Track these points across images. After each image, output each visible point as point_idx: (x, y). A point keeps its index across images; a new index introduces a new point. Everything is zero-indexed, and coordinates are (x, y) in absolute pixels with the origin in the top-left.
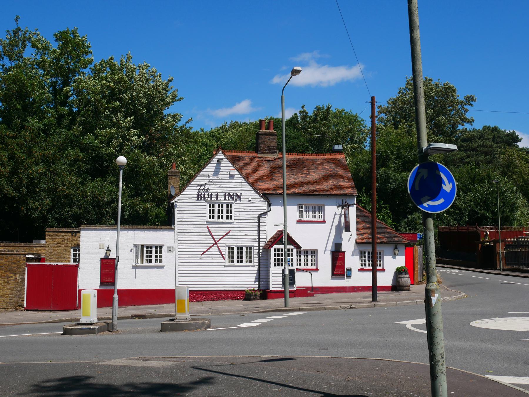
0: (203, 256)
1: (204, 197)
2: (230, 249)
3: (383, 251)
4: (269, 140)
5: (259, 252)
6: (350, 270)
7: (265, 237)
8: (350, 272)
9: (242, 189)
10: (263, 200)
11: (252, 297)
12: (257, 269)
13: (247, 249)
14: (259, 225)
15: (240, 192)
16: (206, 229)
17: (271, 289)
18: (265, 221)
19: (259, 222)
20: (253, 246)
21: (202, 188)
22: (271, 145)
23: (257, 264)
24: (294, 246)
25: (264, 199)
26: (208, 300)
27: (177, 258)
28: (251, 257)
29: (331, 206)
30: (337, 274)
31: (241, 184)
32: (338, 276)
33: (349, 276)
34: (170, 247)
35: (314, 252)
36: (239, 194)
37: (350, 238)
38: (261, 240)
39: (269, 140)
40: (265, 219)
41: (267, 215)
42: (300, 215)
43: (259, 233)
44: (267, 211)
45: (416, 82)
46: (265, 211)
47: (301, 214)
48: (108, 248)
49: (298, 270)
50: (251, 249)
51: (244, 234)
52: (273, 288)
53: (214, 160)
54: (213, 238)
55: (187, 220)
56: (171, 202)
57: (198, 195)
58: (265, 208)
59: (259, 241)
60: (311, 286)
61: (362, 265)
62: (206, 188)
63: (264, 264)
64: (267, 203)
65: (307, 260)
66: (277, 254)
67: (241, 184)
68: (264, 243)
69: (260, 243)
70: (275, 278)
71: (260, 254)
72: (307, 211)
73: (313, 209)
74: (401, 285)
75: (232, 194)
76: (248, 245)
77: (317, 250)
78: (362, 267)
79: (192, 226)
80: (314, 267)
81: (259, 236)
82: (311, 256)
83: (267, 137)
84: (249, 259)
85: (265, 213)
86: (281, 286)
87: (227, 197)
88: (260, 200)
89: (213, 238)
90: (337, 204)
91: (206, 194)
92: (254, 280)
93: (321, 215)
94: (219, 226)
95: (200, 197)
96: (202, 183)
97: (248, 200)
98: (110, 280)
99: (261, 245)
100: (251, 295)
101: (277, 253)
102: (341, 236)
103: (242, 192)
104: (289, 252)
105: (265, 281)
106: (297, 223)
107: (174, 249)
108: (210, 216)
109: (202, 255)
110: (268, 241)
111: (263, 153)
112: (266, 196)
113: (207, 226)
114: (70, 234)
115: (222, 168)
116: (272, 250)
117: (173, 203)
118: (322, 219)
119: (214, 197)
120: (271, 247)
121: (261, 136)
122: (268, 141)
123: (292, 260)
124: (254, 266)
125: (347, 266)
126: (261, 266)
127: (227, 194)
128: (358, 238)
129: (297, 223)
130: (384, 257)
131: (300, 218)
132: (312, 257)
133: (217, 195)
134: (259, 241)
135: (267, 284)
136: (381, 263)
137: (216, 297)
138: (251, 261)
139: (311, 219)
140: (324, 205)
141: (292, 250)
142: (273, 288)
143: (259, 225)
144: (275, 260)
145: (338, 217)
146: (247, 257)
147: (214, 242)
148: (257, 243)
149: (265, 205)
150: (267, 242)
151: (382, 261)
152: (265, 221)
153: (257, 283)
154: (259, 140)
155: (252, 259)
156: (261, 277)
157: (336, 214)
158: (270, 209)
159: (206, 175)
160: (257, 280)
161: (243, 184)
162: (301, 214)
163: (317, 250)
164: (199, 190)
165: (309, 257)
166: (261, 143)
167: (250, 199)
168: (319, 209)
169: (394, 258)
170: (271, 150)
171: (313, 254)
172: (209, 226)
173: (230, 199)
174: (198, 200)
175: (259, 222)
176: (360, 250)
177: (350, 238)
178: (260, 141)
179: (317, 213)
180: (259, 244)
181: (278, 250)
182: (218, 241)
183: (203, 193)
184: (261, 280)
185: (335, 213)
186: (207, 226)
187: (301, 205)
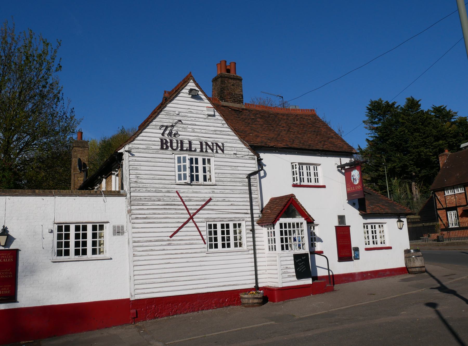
0: (173, 238)
1: (171, 146)
2: (212, 227)
4: (233, 85)
6: (357, 249)
10: (252, 154)
16: (176, 195)
21: (167, 132)
22: (236, 92)
33: (357, 258)
34: (118, 227)
36: (220, 144)
39: (233, 85)
48: (190, 73)
53: (183, 91)
56: (119, 152)
57: (162, 140)
58: (254, 165)
59: (252, 214)
62: (174, 132)
66: (313, 238)
75: (210, 143)
83: (230, 81)
85: (254, 173)
86: (295, 278)
87: (204, 147)
88: (247, 153)
91: (175, 141)
95: (164, 145)
96: (166, 124)
97: (232, 152)
98: (6, 292)
108: (180, 176)
109: (171, 237)
119: (186, 146)
122: (232, 87)
125: (353, 245)
127: (204, 144)
133: (190, 143)
134: (252, 214)
147: (188, 216)
164: (163, 134)
170: (236, 98)
173: (209, 151)
174: (162, 148)
182: (195, 214)
183: (169, 141)
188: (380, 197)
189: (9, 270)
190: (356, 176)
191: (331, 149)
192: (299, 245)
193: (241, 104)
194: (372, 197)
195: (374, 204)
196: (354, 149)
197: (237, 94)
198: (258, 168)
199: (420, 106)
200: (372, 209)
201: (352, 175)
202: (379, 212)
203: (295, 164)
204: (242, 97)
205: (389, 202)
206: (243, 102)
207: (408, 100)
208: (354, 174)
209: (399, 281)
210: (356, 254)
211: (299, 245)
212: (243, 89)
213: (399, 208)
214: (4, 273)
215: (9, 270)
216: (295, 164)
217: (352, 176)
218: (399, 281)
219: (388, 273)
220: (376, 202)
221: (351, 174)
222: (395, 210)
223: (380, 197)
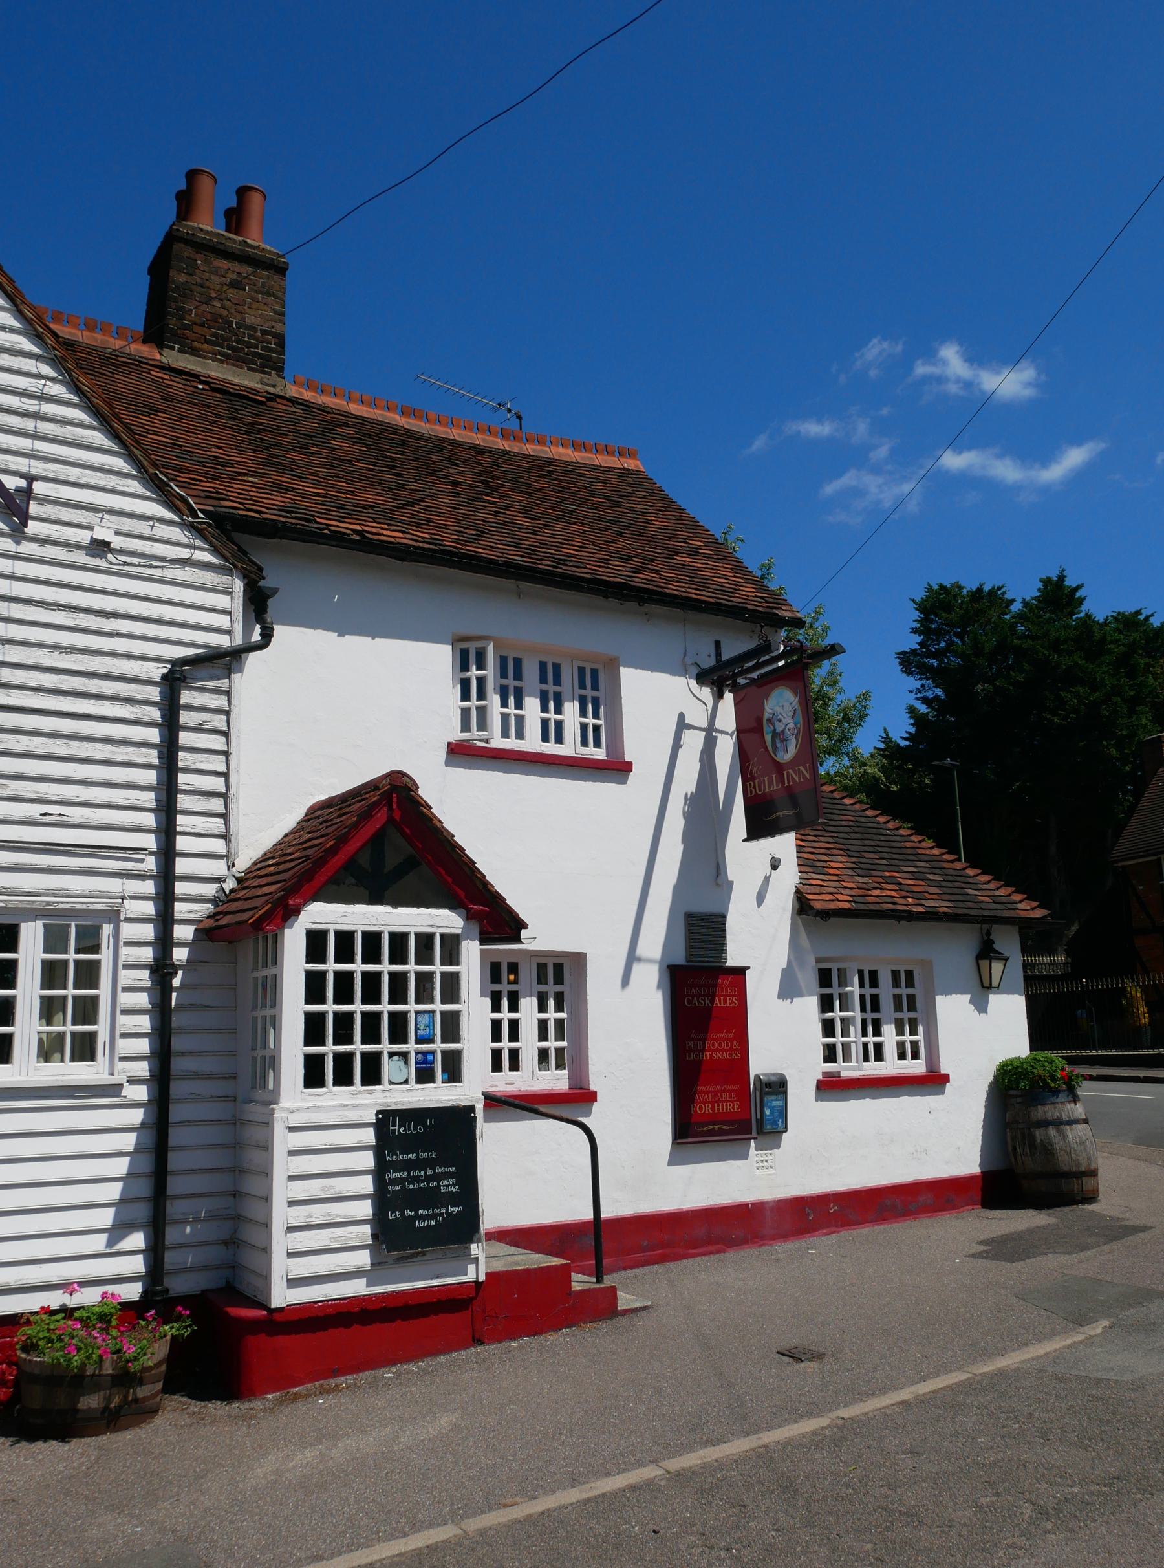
3: (927, 965)
5: (162, 970)
6: (777, 1086)
7: (218, 846)
8: (777, 1103)
9: (40, 445)
11: (91, 1402)
12: (136, 1116)
13: (54, 939)
14: (169, 750)
15: (21, 464)
17: (281, 1296)
18: (218, 722)
19: (170, 725)
20: (114, 916)
22: (250, 319)
23: (142, 1069)
24: (469, 917)
25: (216, 551)
28: (87, 1010)
29: (653, 669)
30: (713, 1119)
31: (32, 405)
32: (712, 1133)
35: (559, 969)
37: (767, 879)
38: (182, 866)
39: (237, 285)
40: (220, 702)
41: (236, 677)
42: (465, 712)
43: (167, 810)
44: (238, 641)
46: (223, 641)
47: (474, 702)
49: (497, 1103)
50: (89, 941)
51: (34, 811)
52: (293, 1283)
58: (222, 621)
59: (166, 878)
60: (589, 1215)
61: (830, 1055)
63: (206, 1065)
64: (239, 585)
65: (514, 1025)
67: (32, 405)
68: (210, 890)
69: (180, 888)
70: (313, 1188)
71: (177, 981)
72: (512, 694)
73: (543, 679)
74: (1066, 1168)
76: (65, 904)
77: (579, 959)
78: (830, 1067)
80: (557, 1080)
81: (167, 832)
82: (534, 1001)
83: (224, 264)
84: (70, 1028)
88: (184, 553)
90: (689, 660)
92: (106, 1218)
93: (597, 728)
97: (84, 537)
99: (180, 909)
100: (79, 1381)
101: (331, 966)
102: (719, 869)
103: (37, 467)
104: (404, 961)
105: (212, 1217)
106: (448, 763)
110: (239, 880)
111: (194, 352)
112: (243, 539)
116: (294, 941)
120: (290, 913)
121: (188, 252)
123: (452, 1026)
124: (114, 1090)
125: (760, 1065)
126: (177, 1089)
128: (804, 882)
129: (448, 763)
130: (940, 999)
131: (466, 727)
132: (542, 1008)
134: (166, 878)
135: (226, 1243)
136: (920, 1037)
138: (85, 1049)
139: (532, 742)
140: (613, 665)
141: (451, 947)
142: (293, 1283)
143: (169, 750)
144: (314, 1029)
145: (694, 742)
146: (50, 1009)
148: (148, 887)
149: (223, 601)
150: (230, 884)
151: (921, 1029)
152: (218, 722)
153: (137, 1240)
154: (173, 273)
155: (102, 1028)
156: (175, 1185)
157: (682, 724)
158: (267, 635)
160: (142, 1211)
161: (48, 408)
162: (474, 702)
163: (579, 959)
165: (528, 1007)
166: (185, 291)
167: (101, 534)
168: (582, 685)
169: (981, 1006)
170: (249, 345)
171: (551, 988)
175: (170, 725)
176: (818, 960)
177: (767, 879)
178: (179, 278)
179: (571, 709)
180: (166, 898)
181: (345, 939)
184: (174, 1209)
185: (682, 716)
187: (472, 647)
188: (908, 844)
189: (731, 1035)
190: (785, 722)
191: (673, 589)
192: (425, 1061)
193: (269, 374)
194: (867, 842)
195: (874, 873)
196: (785, 603)
197: (254, 329)
198: (247, 631)
199: (1081, 601)
200: (861, 892)
201: (766, 716)
202: (891, 906)
203: (479, 644)
204: (281, 344)
205: (946, 865)
206: (281, 369)
207: (1047, 582)
208: (778, 710)
209: (973, 1256)
210: (772, 1109)
211: (425, 1061)
212: (287, 311)
213: (989, 893)
214: (720, 1044)
215: (731, 1035)
216: (479, 644)
217: (769, 721)
218: (973, 1256)
219: (926, 1198)
220: (884, 862)
221: (763, 709)
222: (737, 564)
223: (908, 844)
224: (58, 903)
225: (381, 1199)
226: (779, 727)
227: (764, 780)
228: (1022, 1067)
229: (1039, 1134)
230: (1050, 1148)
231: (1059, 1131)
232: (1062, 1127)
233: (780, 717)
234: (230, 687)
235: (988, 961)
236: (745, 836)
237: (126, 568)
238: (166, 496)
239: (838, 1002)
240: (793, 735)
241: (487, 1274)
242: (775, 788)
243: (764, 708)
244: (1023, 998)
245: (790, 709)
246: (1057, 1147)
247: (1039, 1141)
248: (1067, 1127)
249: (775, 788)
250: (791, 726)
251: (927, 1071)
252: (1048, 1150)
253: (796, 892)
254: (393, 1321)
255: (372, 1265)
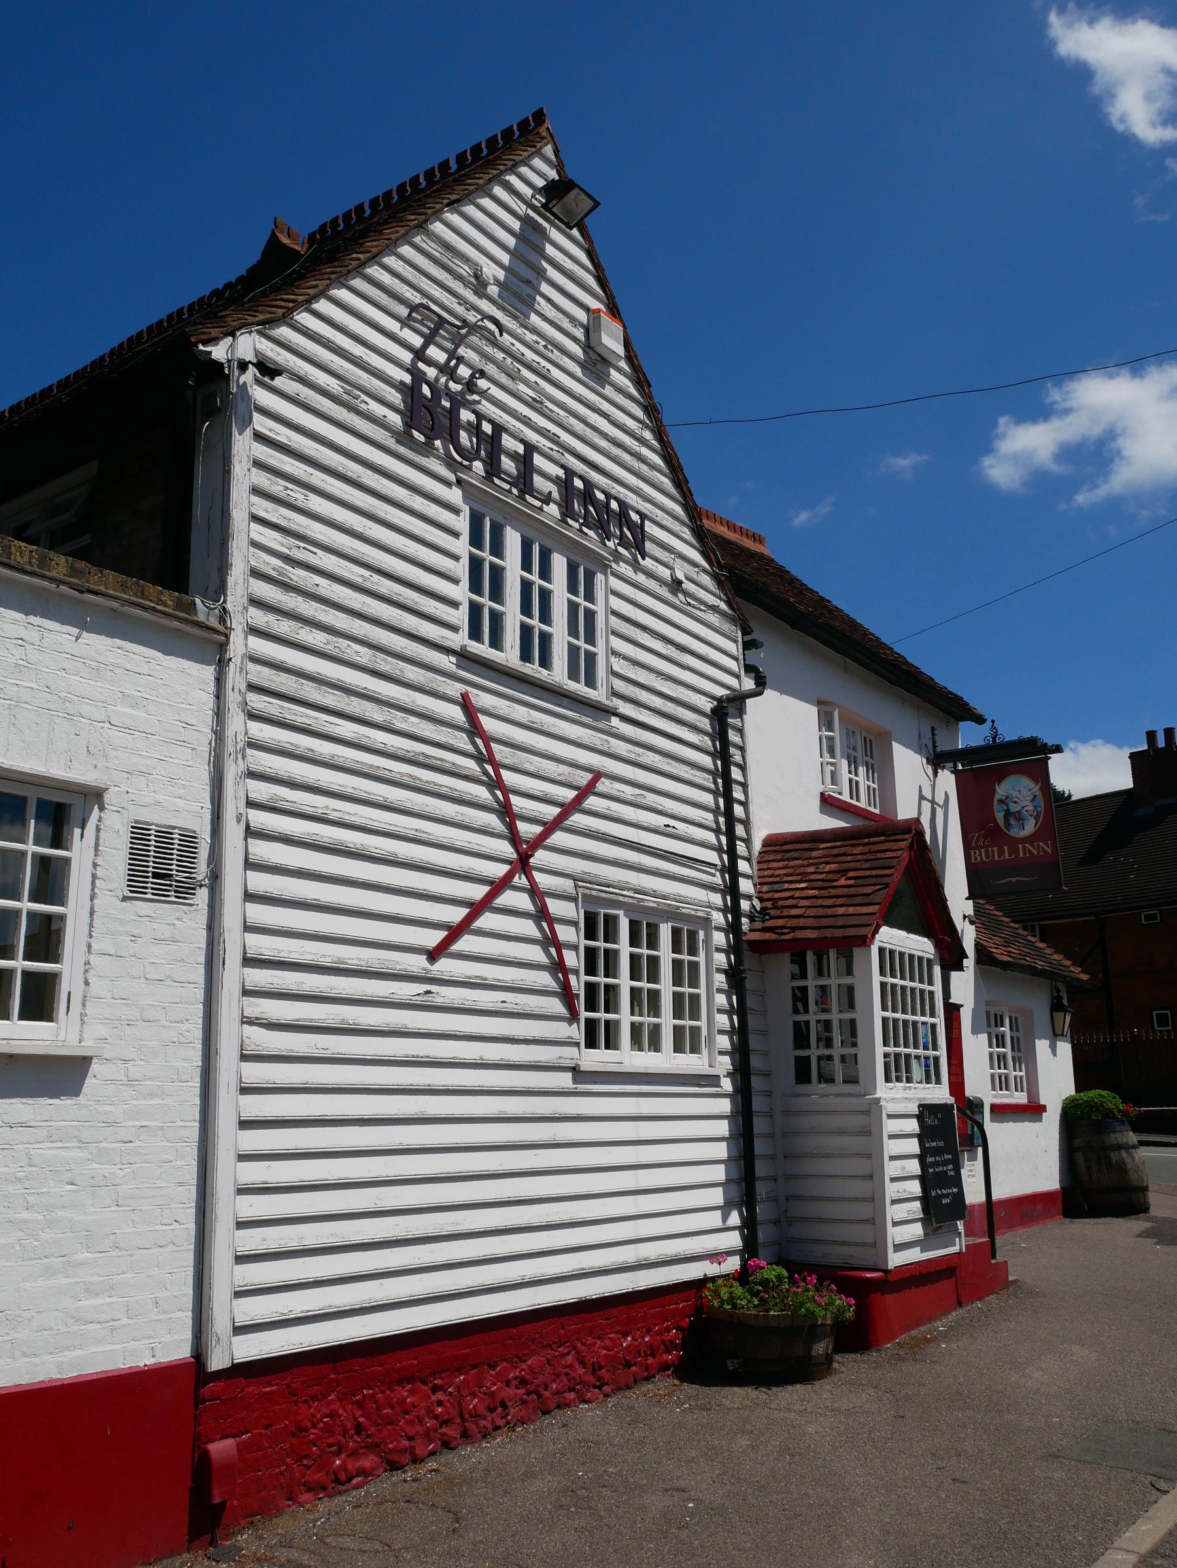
0: (445, 966)
15: (646, 507)
25: (729, 603)
26: (466, 1436)
27: (232, 974)
45: (913, 1277)
51: (659, 821)
54: (505, 812)
55: (326, 587)
79: (364, 655)
89: (505, 812)
94: (537, 716)
107: (202, 869)
109: (433, 955)
113: (465, 696)
114: (13, 645)
115: (498, 191)
117: (216, 372)
118: (1025, 1094)
137: (523, 1382)
153: (735, 1219)
159: (465, 270)
161: (645, 452)
172: (482, 699)
186: (465, 696)
217: (1000, 801)
224: (684, 908)
225: (923, 1179)
226: (1014, 808)
227: (993, 851)
228: (1093, 1101)
229: (1113, 1156)
230: (1124, 1167)
231: (1128, 1153)
232: (1130, 1150)
233: (1016, 799)
234: (743, 726)
235: (1063, 1013)
236: (967, 895)
237: (689, 608)
238: (705, 546)
239: (995, 1040)
240: (1032, 816)
241: (966, 1246)
242: (1007, 857)
243: (995, 790)
244: (1070, 1045)
245: (1029, 794)
246: (1129, 1166)
247: (1114, 1161)
248: (1133, 1150)
249: (1007, 857)
250: (1030, 808)
251: (1029, 1102)
252: (1122, 1168)
253: (976, 945)
254: (926, 1285)
255: (925, 1235)
